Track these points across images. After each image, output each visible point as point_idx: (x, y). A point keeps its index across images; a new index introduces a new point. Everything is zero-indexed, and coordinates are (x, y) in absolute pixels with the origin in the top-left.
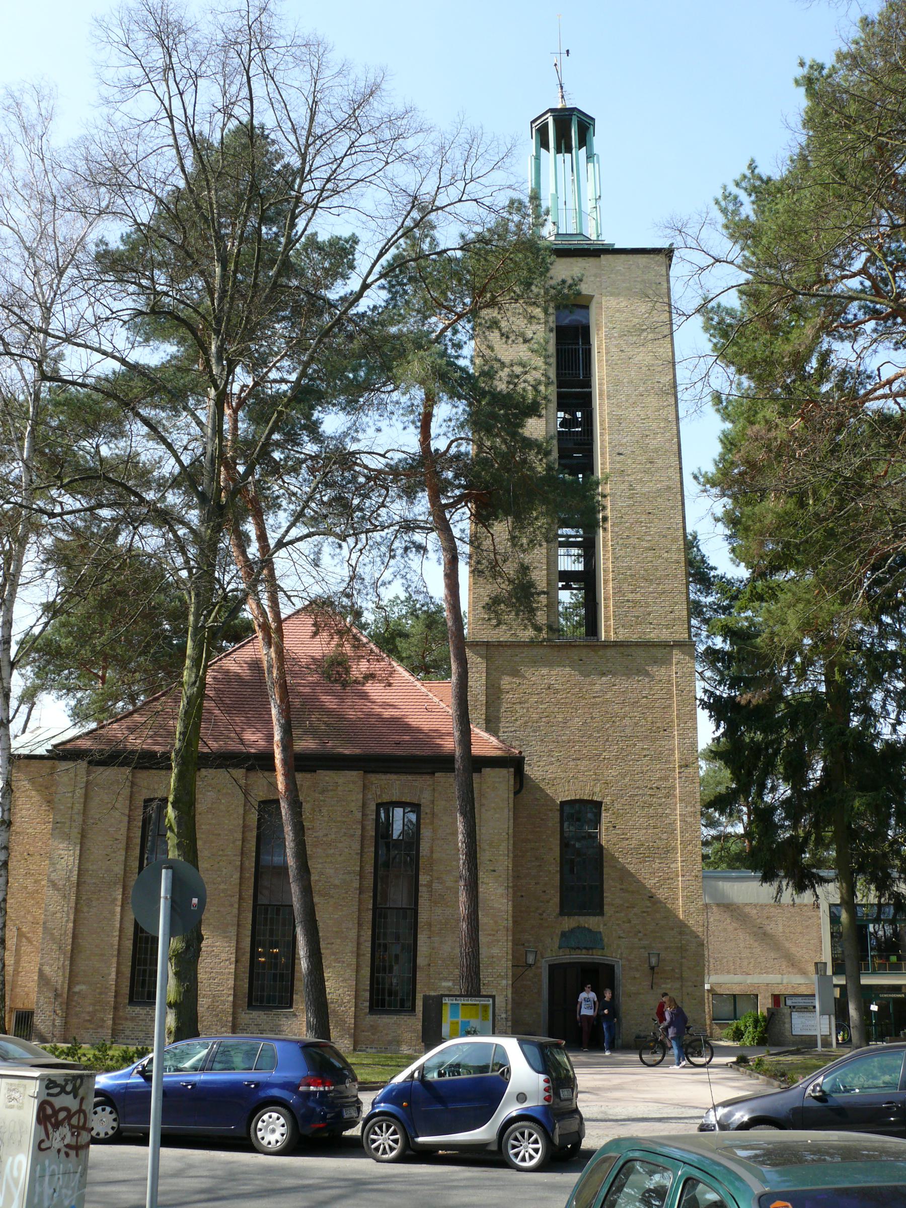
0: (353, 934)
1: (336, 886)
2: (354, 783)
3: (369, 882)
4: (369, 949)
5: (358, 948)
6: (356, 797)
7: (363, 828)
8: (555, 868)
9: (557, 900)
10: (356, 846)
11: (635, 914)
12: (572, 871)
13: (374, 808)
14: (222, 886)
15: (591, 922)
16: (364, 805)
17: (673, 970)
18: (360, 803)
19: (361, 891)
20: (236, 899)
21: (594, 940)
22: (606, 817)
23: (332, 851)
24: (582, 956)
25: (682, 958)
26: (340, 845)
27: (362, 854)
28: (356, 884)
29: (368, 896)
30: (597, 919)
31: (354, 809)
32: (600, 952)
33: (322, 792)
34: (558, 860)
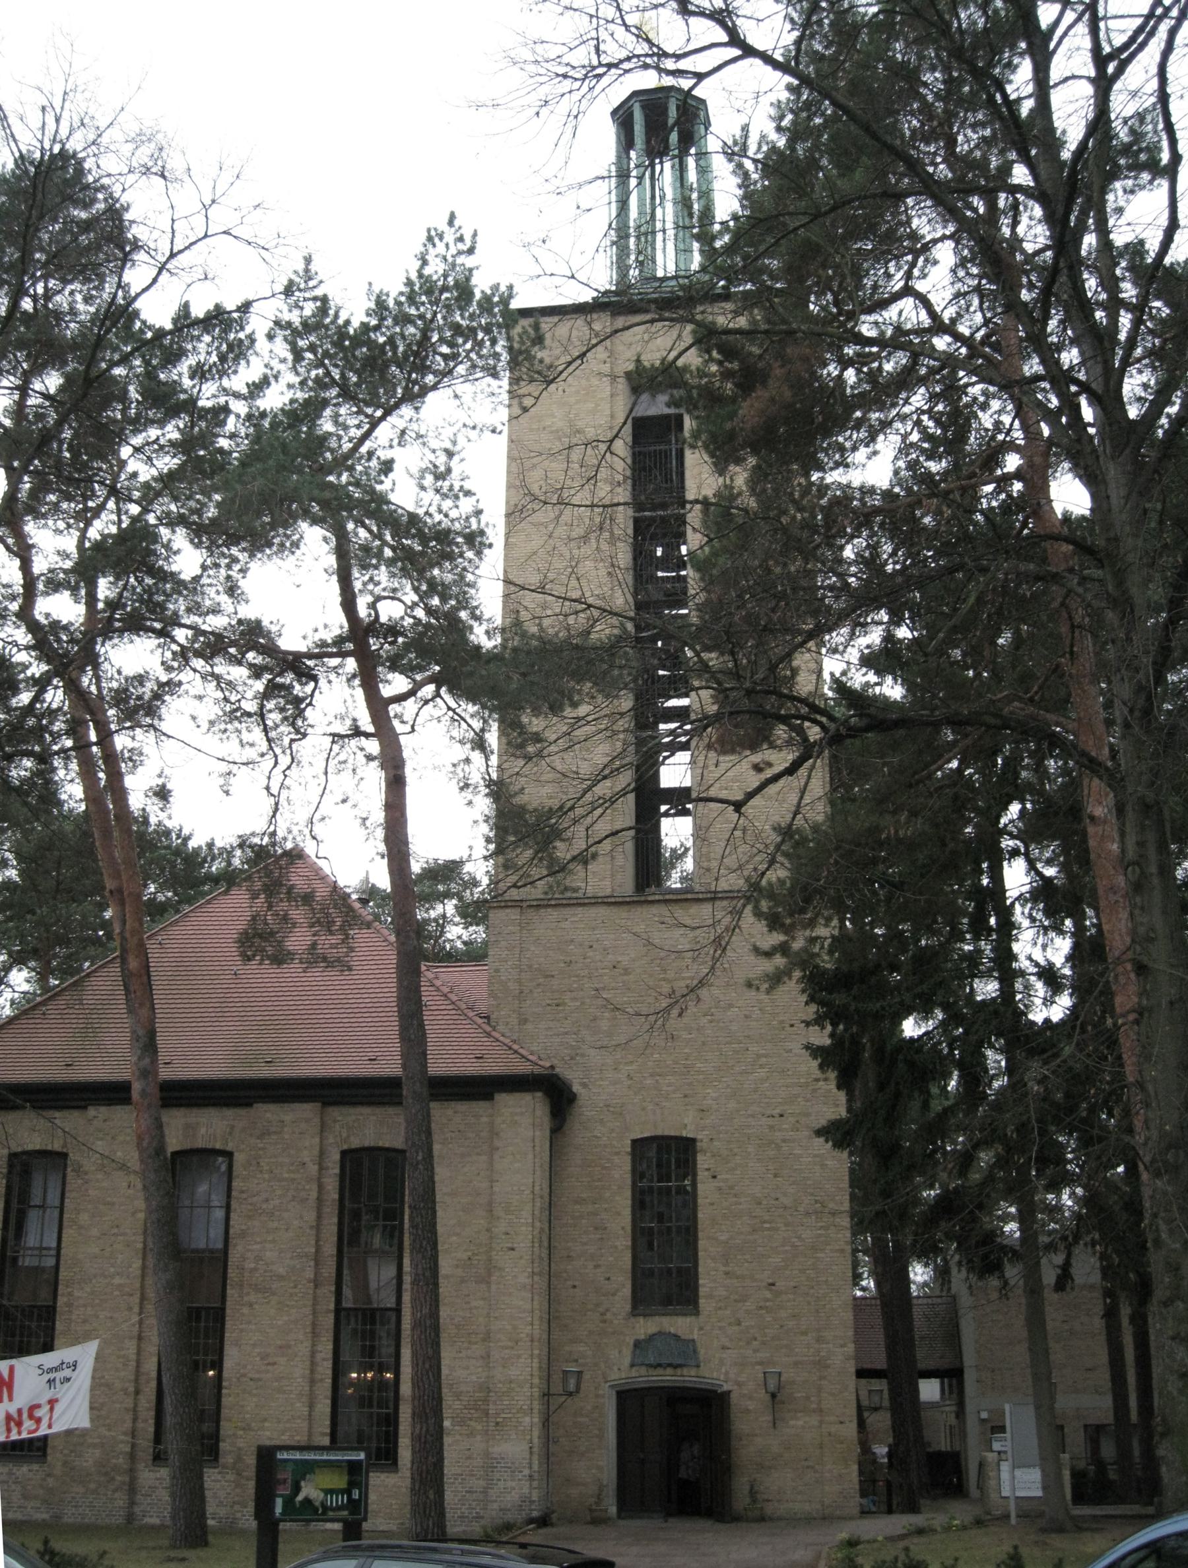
0: (304, 1349)
1: (281, 1278)
2: (307, 1121)
3: (329, 1269)
4: (329, 1372)
5: (312, 1371)
6: (311, 1142)
7: (321, 1187)
8: (623, 1242)
9: (627, 1291)
10: (311, 1216)
11: (748, 1312)
12: (650, 1246)
13: (337, 1157)
14: (117, 1281)
15: (679, 1325)
16: (322, 1153)
17: (808, 1398)
18: (316, 1152)
19: (317, 1283)
20: (136, 1299)
21: (686, 1351)
22: (703, 1162)
23: (275, 1224)
24: (667, 1377)
25: (821, 1378)
26: (286, 1215)
27: (318, 1227)
28: (309, 1274)
29: (327, 1292)
30: (688, 1319)
31: (306, 1159)
32: (693, 1372)
33: (261, 1137)
34: (629, 1228)
